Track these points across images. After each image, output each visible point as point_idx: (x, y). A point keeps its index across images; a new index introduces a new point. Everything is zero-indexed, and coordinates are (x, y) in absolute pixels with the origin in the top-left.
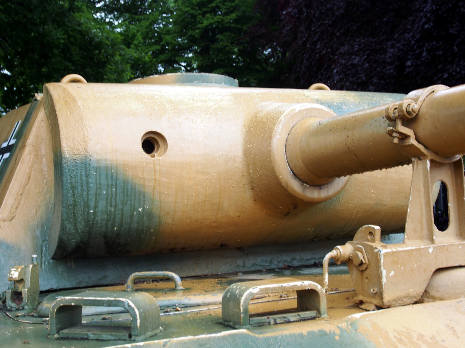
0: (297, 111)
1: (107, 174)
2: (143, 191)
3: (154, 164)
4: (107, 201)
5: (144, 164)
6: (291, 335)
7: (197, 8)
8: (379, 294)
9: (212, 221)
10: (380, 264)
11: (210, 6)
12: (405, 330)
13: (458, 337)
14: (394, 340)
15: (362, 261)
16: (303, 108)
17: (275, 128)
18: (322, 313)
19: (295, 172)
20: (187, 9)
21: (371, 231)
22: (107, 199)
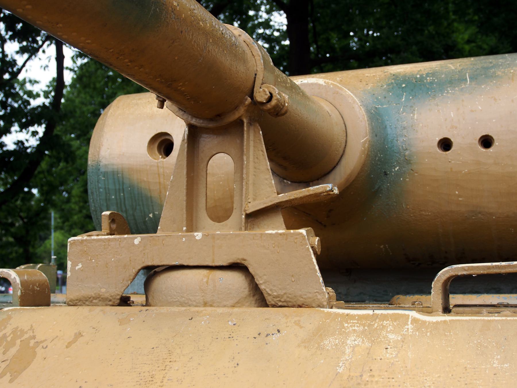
1: (114, 179)
2: (149, 195)
3: (158, 166)
4: (117, 206)
5: (148, 167)
22: (117, 204)
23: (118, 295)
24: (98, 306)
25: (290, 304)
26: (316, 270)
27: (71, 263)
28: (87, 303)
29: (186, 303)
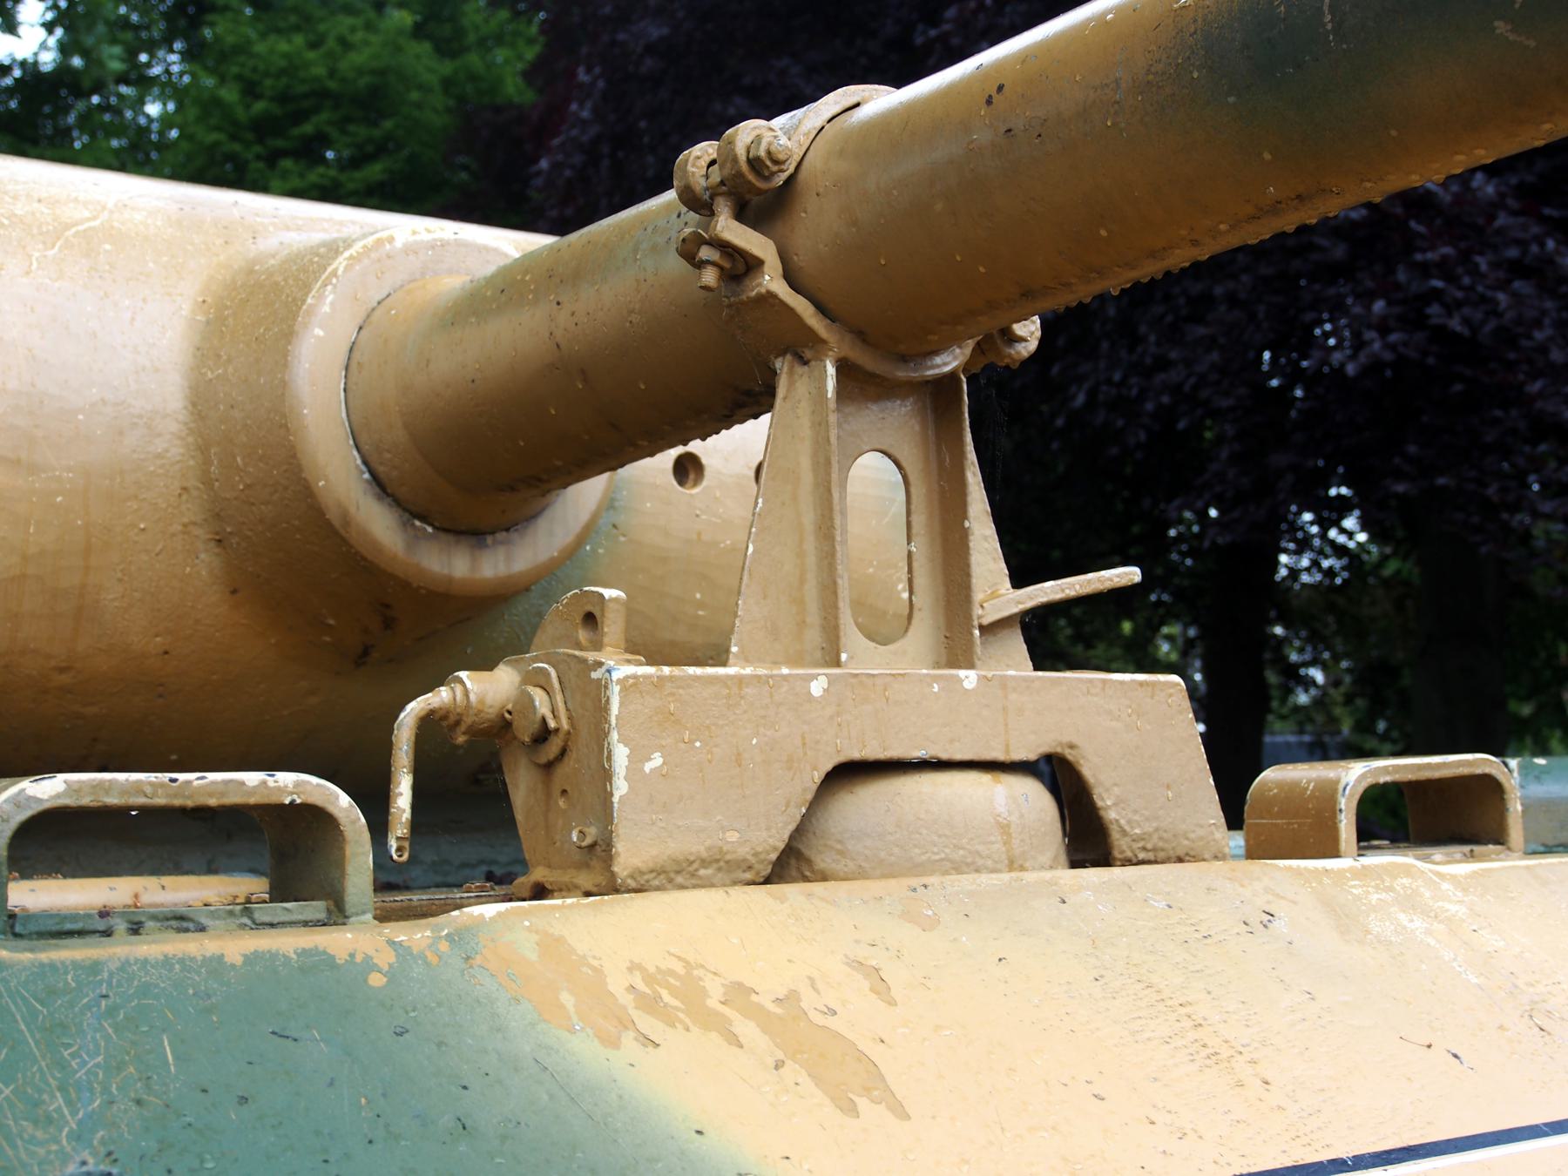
0: (398, 244)
6: (167, 962)
7: (250, 136)
8: (599, 852)
9: (53, 663)
10: (607, 721)
11: (296, 131)
12: (679, 968)
13: (892, 1003)
14: (627, 999)
15: (544, 719)
16: (426, 237)
17: (309, 301)
18: (349, 909)
19: (381, 469)
20: (214, 137)
21: (589, 608)
23: (775, 849)
24: (713, 885)
25: (1161, 855)
26: (318, 785)
27: (626, 751)
28: (679, 879)
29: (968, 865)
